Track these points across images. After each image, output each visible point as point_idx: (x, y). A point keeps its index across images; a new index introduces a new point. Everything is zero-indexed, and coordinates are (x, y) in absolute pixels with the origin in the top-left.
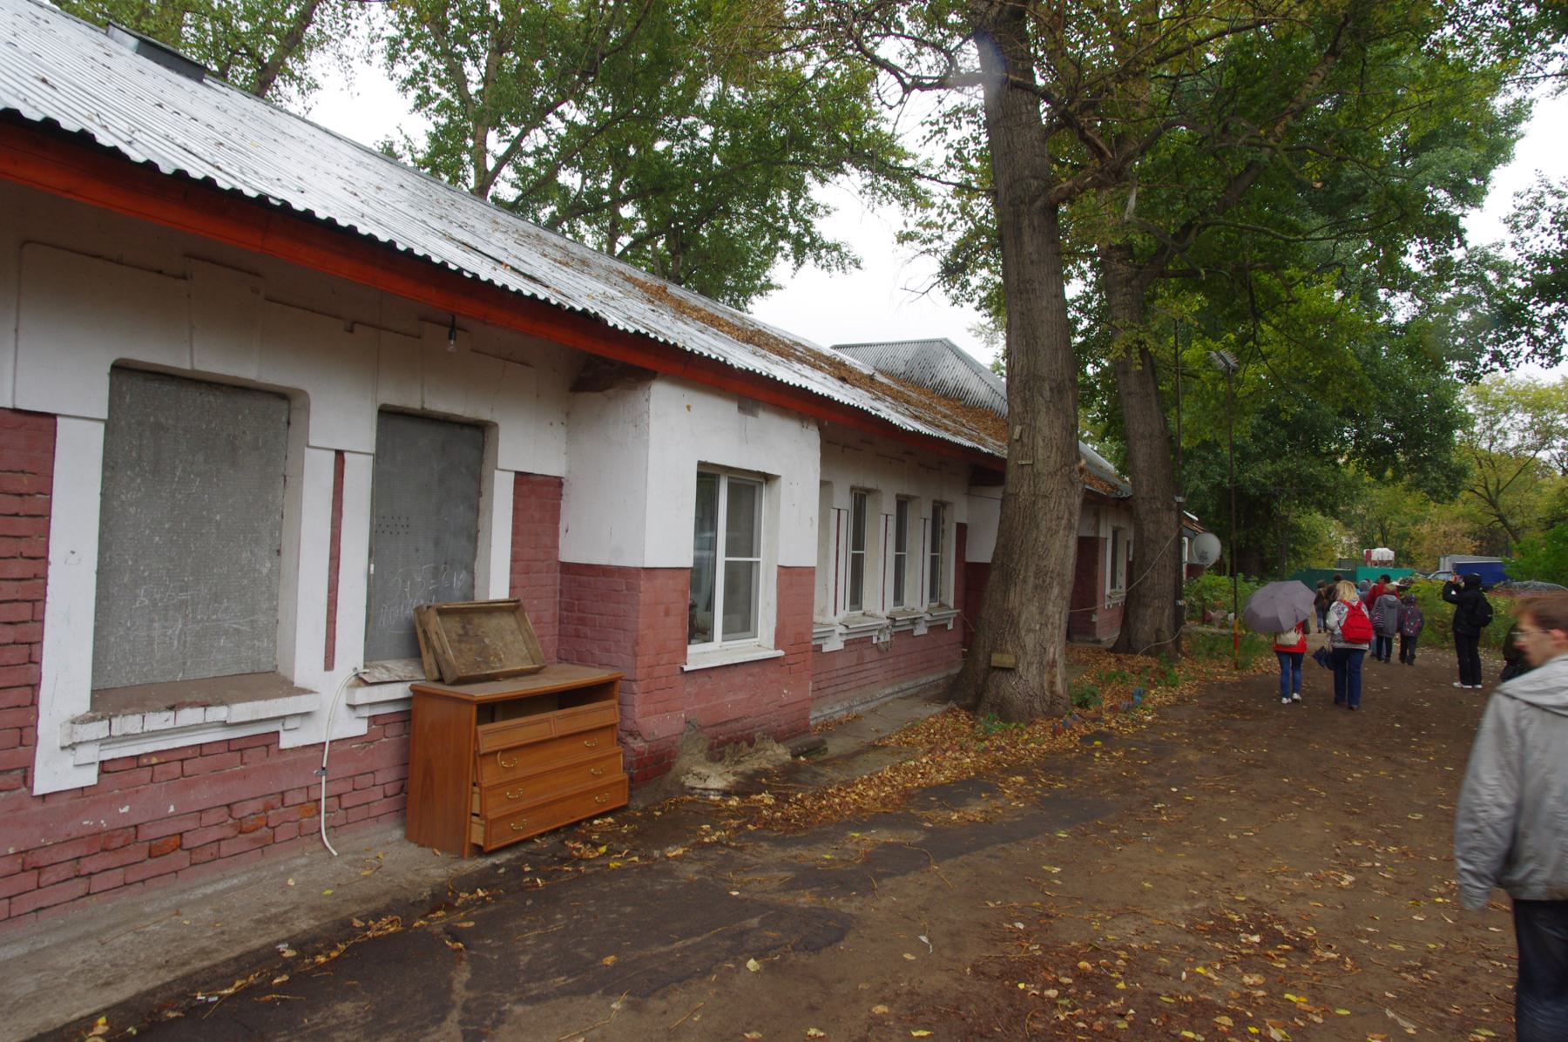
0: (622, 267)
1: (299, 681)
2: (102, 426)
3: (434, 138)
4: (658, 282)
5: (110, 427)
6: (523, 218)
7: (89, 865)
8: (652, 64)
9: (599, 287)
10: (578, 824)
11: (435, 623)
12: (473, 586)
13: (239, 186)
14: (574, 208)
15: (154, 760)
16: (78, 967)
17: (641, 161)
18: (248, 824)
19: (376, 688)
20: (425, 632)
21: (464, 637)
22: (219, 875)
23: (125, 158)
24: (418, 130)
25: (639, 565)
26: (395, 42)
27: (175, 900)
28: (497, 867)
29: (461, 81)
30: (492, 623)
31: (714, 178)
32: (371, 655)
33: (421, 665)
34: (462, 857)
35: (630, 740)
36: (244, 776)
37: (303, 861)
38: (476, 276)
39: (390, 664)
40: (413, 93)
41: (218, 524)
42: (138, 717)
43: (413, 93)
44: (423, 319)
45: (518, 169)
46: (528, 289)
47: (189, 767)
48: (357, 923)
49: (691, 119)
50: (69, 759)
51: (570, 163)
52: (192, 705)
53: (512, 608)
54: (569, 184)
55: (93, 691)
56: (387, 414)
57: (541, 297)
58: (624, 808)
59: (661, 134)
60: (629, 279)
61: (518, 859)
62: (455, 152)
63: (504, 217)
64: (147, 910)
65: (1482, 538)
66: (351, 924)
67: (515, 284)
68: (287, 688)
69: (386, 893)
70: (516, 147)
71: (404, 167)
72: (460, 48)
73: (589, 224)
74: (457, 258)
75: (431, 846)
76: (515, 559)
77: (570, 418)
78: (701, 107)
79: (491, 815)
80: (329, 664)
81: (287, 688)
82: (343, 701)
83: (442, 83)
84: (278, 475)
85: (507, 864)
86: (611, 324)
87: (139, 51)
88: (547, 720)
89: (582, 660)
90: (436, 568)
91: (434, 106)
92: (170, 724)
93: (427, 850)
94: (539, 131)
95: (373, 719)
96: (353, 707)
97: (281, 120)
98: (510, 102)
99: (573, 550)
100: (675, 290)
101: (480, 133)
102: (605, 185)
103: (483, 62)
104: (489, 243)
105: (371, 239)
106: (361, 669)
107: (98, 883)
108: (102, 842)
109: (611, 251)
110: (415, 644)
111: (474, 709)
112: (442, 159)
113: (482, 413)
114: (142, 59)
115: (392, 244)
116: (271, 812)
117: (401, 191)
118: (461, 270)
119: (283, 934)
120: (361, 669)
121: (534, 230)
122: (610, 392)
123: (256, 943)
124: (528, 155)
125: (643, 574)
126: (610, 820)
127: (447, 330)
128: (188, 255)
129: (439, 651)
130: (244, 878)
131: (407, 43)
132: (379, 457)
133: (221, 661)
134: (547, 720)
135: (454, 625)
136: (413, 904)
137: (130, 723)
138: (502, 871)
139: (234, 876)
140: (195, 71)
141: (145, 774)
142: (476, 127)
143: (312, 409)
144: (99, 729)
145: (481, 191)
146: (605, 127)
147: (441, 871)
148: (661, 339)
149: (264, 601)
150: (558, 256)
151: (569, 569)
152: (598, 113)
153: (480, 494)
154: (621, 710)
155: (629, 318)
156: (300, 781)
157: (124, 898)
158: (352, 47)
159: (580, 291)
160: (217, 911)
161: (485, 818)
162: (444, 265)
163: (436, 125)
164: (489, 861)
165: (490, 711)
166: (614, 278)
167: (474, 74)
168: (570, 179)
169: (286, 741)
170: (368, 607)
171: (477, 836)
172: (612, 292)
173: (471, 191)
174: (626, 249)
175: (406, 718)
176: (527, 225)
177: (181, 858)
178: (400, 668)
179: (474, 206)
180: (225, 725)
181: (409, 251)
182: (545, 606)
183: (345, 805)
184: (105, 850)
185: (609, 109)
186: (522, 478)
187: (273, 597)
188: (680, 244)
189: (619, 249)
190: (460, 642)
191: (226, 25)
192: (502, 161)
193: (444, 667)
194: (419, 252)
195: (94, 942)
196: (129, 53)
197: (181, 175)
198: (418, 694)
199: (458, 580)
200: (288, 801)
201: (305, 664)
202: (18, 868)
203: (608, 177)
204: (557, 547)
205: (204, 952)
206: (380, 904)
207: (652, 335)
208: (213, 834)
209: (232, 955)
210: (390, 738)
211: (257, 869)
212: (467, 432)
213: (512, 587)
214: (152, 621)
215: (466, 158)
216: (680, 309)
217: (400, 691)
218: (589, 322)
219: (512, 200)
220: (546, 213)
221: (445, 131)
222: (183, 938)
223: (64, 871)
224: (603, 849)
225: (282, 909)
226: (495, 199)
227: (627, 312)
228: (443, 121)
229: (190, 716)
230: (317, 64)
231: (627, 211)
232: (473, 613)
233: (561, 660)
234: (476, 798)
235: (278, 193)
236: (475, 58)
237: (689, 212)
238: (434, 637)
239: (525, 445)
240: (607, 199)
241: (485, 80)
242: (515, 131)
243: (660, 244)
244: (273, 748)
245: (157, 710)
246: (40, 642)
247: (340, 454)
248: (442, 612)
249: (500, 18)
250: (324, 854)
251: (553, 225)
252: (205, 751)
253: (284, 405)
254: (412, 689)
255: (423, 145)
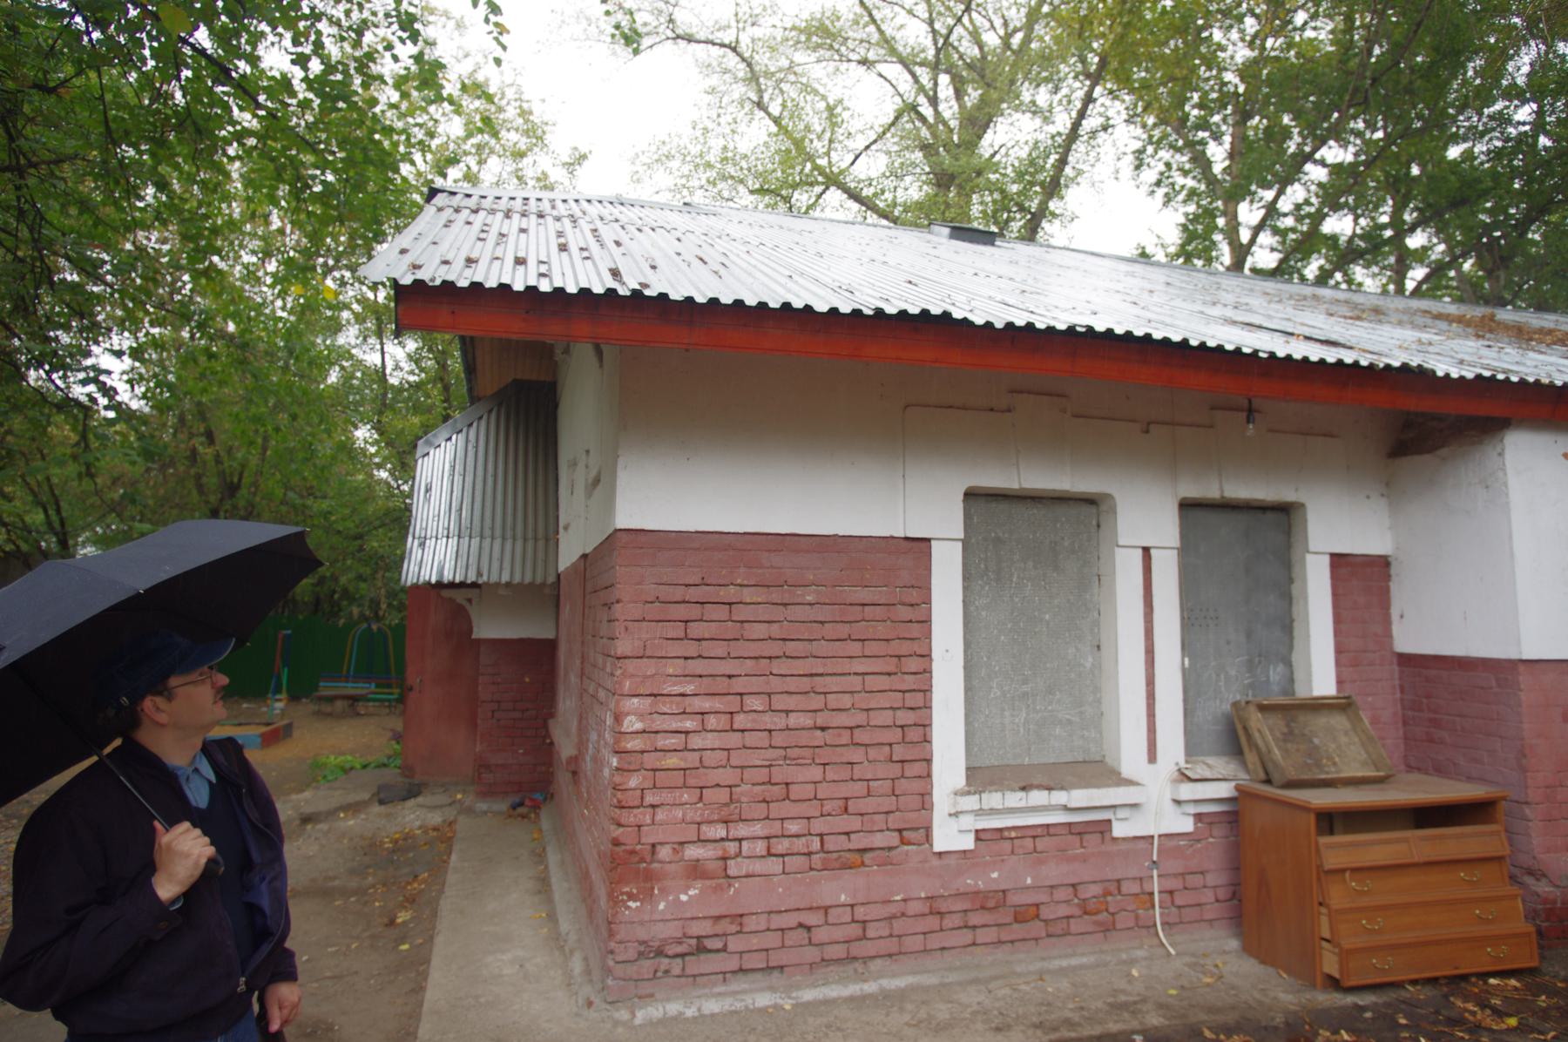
0: (1416, 304)
1: (1126, 771)
2: (960, 544)
3: (1185, 228)
4: (1479, 311)
5: (966, 543)
6: (1290, 281)
7: (975, 919)
8: (1432, 63)
9: (1409, 335)
10: (1464, 978)
11: (1256, 720)
12: (1292, 681)
13: (1052, 323)
14: (1345, 255)
15: (1013, 834)
16: (975, 1007)
17: (1431, 178)
18: (1091, 906)
19: (1199, 785)
20: (1245, 729)
21: (1288, 736)
22: (1070, 951)
23: (972, 323)
24: (1165, 225)
25: (1514, 655)
26: (1140, 152)
27: (1038, 965)
28: (1363, 1009)
29: (1202, 162)
30: (1321, 721)
31: (1546, 164)
32: (1191, 750)
33: (1244, 764)
34: (1313, 986)
35: (1529, 880)
36: (1084, 859)
37: (1140, 953)
38: (1272, 355)
39: (1211, 760)
40: (1161, 192)
41: (1048, 623)
42: (999, 794)
43: (1161, 192)
44: (1213, 408)
45: (1276, 231)
46: (1331, 356)
47: (1041, 844)
48: (1207, 1034)
49: (1498, 106)
50: (954, 825)
51: (1336, 207)
52: (1040, 787)
53: (1341, 705)
54: (1337, 230)
55: (968, 769)
56: (1186, 506)
57: (1348, 360)
58: (1531, 971)
59: (1455, 139)
60: (1439, 317)
61: (1387, 1005)
62: (1207, 236)
63: (1271, 285)
64: (1018, 969)
65: (215, 231)
66: (1201, 1034)
67: (1315, 353)
68: (1114, 778)
69: (1233, 1008)
70: (1271, 210)
71: (1158, 264)
72: (1201, 134)
73: (1367, 267)
74: (1249, 341)
75: (1273, 965)
76: (1339, 650)
77: (1391, 489)
78: (1514, 85)
79: (1347, 943)
80: (1152, 757)
81: (1114, 778)
82: (1168, 796)
83: (1185, 173)
84: (1090, 577)
85: (1372, 1007)
86: (1440, 374)
87: (952, 237)
88: (1406, 840)
89: (1440, 770)
90: (1250, 661)
91: (1181, 197)
92: (1023, 804)
93: (1271, 970)
94: (1297, 186)
95: (1198, 817)
96: (1178, 802)
97: (1055, 256)
98: (1262, 164)
99: (1411, 637)
100: (1506, 315)
101: (1231, 209)
102: (1385, 219)
103: (1227, 139)
104: (1270, 317)
105: (1166, 341)
106: (1183, 764)
107: (983, 935)
108: (986, 901)
109: (1400, 289)
110: (1234, 739)
111: (1312, 817)
112: (1195, 245)
113: (1287, 494)
114: (954, 242)
115: (1185, 341)
116: (1109, 898)
117: (1171, 290)
118: (1256, 352)
119: (1135, 1024)
120: (1183, 764)
121: (1308, 291)
122: (1444, 452)
123: (1113, 1027)
124: (1285, 215)
125: (1521, 668)
126: (1513, 982)
127: (1245, 414)
128: (1011, 392)
129: (1264, 749)
130: (1092, 959)
131: (1150, 149)
132: (1186, 550)
133: (1057, 750)
134: (1406, 840)
135: (1277, 721)
136: (1266, 1028)
137: (993, 799)
138: (1368, 1015)
139: (1083, 954)
140: (986, 238)
141: (1007, 845)
142: (1225, 204)
143: (1119, 509)
144: (971, 802)
145: (1237, 266)
146: (1375, 156)
147: (1289, 998)
148: (1515, 379)
149: (1087, 693)
150: (1344, 310)
151: (1407, 660)
152: (1368, 143)
153: (1291, 581)
154: (1510, 841)
155: (1461, 362)
156: (1133, 872)
157: (1001, 954)
158: (1103, 171)
159: (1388, 343)
160: (1074, 985)
161: (1338, 945)
162: (1238, 351)
163: (1186, 215)
164: (1350, 999)
165: (1329, 821)
166: (1420, 320)
167: (1218, 154)
168: (1340, 225)
169: (1119, 830)
170: (1185, 701)
171: (1330, 965)
172: (1425, 336)
173: (1228, 269)
174: (1420, 283)
175: (1233, 818)
176: (1296, 288)
177: (1036, 927)
178: (1221, 765)
179: (1232, 282)
180: (1066, 808)
181: (1203, 345)
182: (1383, 700)
183: (1178, 902)
184: (983, 908)
185: (1379, 135)
186: (1339, 562)
187: (1097, 690)
188: (1496, 259)
189: (1410, 285)
190: (1285, 741)
191: (1002, 191)
192: (1257, 230)
193: (1271, 768)
194: (1211, 343)
195: (982, 987)
196: (945, 240)
197: (1010, 326)
198: (1243, 795)
199: (1276, 673)
200: (1124, 890)
201: (1130, 756)
202: (927, 911)
203: (1388, 207)
204: (1390, 636)
205: (1068, 1023)
206: (1230, 1018)
207: (1500, 377)
208: (1063, 910)
209: (1093, 1033)
210: (1217, 838)
211: (1102, 952)
212: (1270, 516)
213: (1340, 682)
214: (1003, 710)
215: (1218, 237)
216: (1523, 336)
217: (1224, 790)
218: (1413, 378)
219: (1273, 265)
220: (1311, 270)
221: (1195, 219)
222: (1049, 1004)
223: (956, 920)
224: (1513, 1022)
225: (1131, 999)
226: (1254, 270)
227: (1455, 355)
228: (1192, 208)
229: (1038, 797)
230: (1073, 199)
231: (1415, 241)
232: (1297, 711)
233: (1410, 768)
234: (1324, 921)
235: (1082, 320)
236: (1217, 137)
237: (1509, 217)
238: (1257, 735)
239: (1339, 523)
240: (1388, 233)
241: (1231, 156)
242: (1269, 195)
243: (1467, 266)
244: (1107, 835)
245: (1013, 790)
246: (930, 725)
247: (1146, 550)
248: (1262, 708)
249: (1241, 89)
250: (1160, 951)
251: (1323, 278)
252: (1052, 831)
253: (1093, 509)
254: (1237, 788)
255: (1174, 238)
